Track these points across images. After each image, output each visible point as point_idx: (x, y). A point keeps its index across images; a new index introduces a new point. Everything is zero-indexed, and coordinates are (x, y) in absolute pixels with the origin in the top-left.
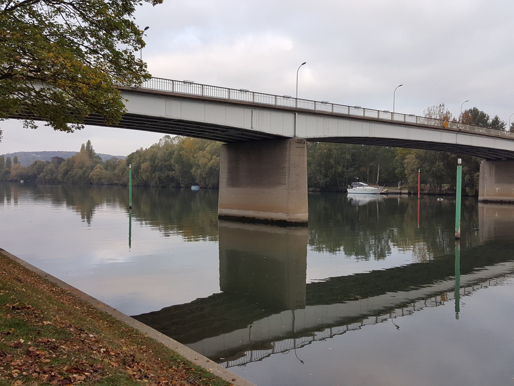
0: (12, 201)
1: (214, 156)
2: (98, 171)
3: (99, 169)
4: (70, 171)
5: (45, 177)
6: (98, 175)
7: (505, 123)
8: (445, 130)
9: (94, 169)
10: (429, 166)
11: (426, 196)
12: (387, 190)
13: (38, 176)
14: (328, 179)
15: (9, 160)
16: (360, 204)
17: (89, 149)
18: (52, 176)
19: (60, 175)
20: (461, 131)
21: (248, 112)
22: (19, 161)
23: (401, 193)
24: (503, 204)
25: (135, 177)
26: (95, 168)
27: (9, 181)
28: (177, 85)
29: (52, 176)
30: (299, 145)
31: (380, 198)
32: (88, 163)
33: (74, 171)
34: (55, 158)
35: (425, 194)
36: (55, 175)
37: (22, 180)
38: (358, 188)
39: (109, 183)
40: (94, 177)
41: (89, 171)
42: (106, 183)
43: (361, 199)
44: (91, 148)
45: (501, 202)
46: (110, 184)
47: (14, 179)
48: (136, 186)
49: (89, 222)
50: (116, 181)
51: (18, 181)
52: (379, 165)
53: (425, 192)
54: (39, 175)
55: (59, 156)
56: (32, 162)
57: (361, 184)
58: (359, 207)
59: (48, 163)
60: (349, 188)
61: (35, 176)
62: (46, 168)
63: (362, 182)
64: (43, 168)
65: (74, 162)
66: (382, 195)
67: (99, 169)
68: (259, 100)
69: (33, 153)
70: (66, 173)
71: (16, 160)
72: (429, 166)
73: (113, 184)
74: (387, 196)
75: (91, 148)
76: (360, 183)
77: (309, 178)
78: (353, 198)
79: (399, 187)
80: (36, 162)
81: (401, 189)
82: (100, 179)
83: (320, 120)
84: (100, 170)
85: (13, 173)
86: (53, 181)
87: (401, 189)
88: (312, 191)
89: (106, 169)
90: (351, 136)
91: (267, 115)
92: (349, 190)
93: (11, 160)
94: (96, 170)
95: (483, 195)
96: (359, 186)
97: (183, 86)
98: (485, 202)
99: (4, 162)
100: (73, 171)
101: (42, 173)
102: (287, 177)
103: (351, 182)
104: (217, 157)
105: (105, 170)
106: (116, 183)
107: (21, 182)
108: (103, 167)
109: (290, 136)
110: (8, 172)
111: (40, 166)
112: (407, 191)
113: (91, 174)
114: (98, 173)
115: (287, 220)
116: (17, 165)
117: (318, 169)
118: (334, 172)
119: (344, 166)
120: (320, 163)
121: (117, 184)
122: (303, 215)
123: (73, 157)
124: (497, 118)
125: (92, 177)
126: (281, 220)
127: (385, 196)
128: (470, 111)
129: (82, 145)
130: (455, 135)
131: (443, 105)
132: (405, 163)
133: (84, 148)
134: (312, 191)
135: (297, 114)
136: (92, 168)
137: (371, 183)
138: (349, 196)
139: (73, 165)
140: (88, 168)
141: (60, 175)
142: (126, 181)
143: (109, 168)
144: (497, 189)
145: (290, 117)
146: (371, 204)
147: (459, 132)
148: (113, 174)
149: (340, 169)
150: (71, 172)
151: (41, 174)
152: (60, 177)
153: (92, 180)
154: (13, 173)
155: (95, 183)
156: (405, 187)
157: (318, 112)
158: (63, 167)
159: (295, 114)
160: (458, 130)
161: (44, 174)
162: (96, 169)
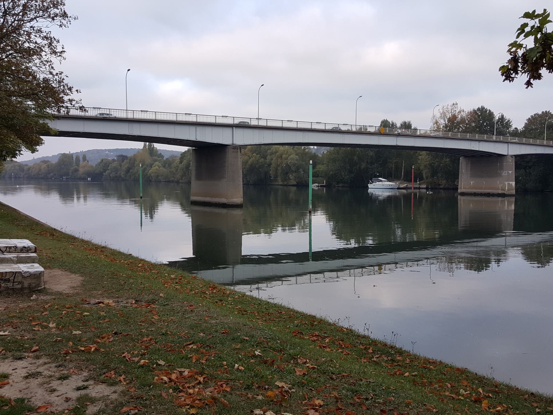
0: (82, 200)
1: (254, 154)
2: (157, 169)
3: (157, 167)
4: (132, 169)
5: (110, 175)
6: (156, 173)
7: (511, 120)
8: (381, 134)
9: (153, 166)
10: (438, 162)
11: (441, 191)
12: (406, 185)
13: (104, 173)
14: (353, 175)
15: (78, 158)
16: (380, 198)
17: (151, 147)
18: (116, 173)
19: (122, 173)
20: (400, 134)
21: (193, 128)
22: (87, 159)
23: (419, 188)
24: (483, 197)
25: (187, 174)
26: (154, 165)
27: (77, 179)
28: (136, 113)
29: (116, 173)
30: (234, 150)
31: (397, 193)
32: (148, 161)
33: (21, 172)
34: (119, 156)
35: (441, 189)
36: (119, 173)
37: (89, 178)
38: (377, 183)
39: (166, 180)
40: (152, 175)
41: (148, 168)
42: (163, 181)
43: (380, 194)
44: (152, 147)
45: (475, 194)
46: (166, 181)
47: (82, 176)
48: (187, 183)
49: (152, 217)
50: (173, 179)
51: (86, 179)
52: (404, 162)
53: (441, 187)
54: (105, 172)
55: (123, 154)
56: (99, 161)
57: (380, 180)
58: (380, 201)
59: (114, 160)
60: (371, 183)
61: (101, 174)
62: (111, 166)
63: (382, 177)
64: (108, 166)
65: (135, 160)
66: (399, 190)
67: (157, 167)
68: (201, 120)
69: (106, 150)
70: (128, 170)
71: (84, 158)
72: (438, 162)
73: (169, 182)
74: (407, 191)
75: (152, 147)
76: (379, 178)
77: (515, 177)
78: (374, 193)
79: (418, 182)
80: (102, 160)
81: (420, 184)
82: (158, 176)
83: (256, 132)
84: (158, 167)
85: (81, 170)
86: (117, 179)
87: (420, 184)
88: (341, 187)
89: (164, 167)
90: (285, 142)
91: (208, 129)
92: (370, 186)
93: (80, 157)
94: (154, 168)
95: (461, 188)
96: (378, 182)
97: (141, 114)
98: (463, 194)
99: (73, 160)
100: (134, 169)
101: (107, 171)
102: (227, 173)
103: (373, 177)
104: (257, 155)
105: (162, 168)
106: (172, 180)
107: (89, 180)
108: (161, 164)
109: (229, 144)
110: (76, 170)
111: (106, 164)
112: (425, 186)
113: (150, 171)
114: (156, 171)
115: (227, 203)
116: (85, 163)
117: (342, 166)
118: (358, 168)
119: (367, 162)
120: (345, 160)
121: (173, 182)
122: (238, 199)
123: (135, 155)
124: (503, 116)
125: (150, 175)
126: (224, 203)
127: (404, 191)
128: (479, 109)
129: (532, 84)
130: (396, 138)
131: (457, 104)
132: (419, 160)
133: (146, 146)
134: (341, 187)
135: (234, 128)
136: (151, 166)
137: (389, 177)
138: (370, 191)
139: (135, 163)
140: (147, 166)
141: (122, 173)
142: (179, 178)
143: (167, 165)
144: (472, 182)
145: (229, 130)
146: (389, 198)
147: (399, 135)
148: (170, 172)
149: (363, 166)
150: (133, 170)
151: (107, 172)
152: (124, 174)
153: (150, 178)
154: (81, 170)
155: (153, 180)
156: (424, 183)
157: (253, 126)
158: (125, 165)
159: (233, 128)
160: (397, 134)
161: (109, 171)
162: (154, 167)
